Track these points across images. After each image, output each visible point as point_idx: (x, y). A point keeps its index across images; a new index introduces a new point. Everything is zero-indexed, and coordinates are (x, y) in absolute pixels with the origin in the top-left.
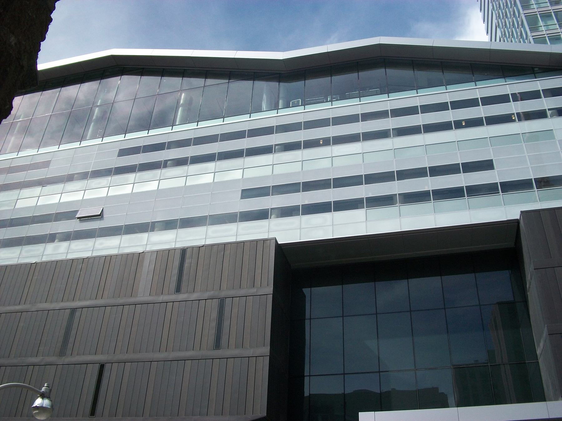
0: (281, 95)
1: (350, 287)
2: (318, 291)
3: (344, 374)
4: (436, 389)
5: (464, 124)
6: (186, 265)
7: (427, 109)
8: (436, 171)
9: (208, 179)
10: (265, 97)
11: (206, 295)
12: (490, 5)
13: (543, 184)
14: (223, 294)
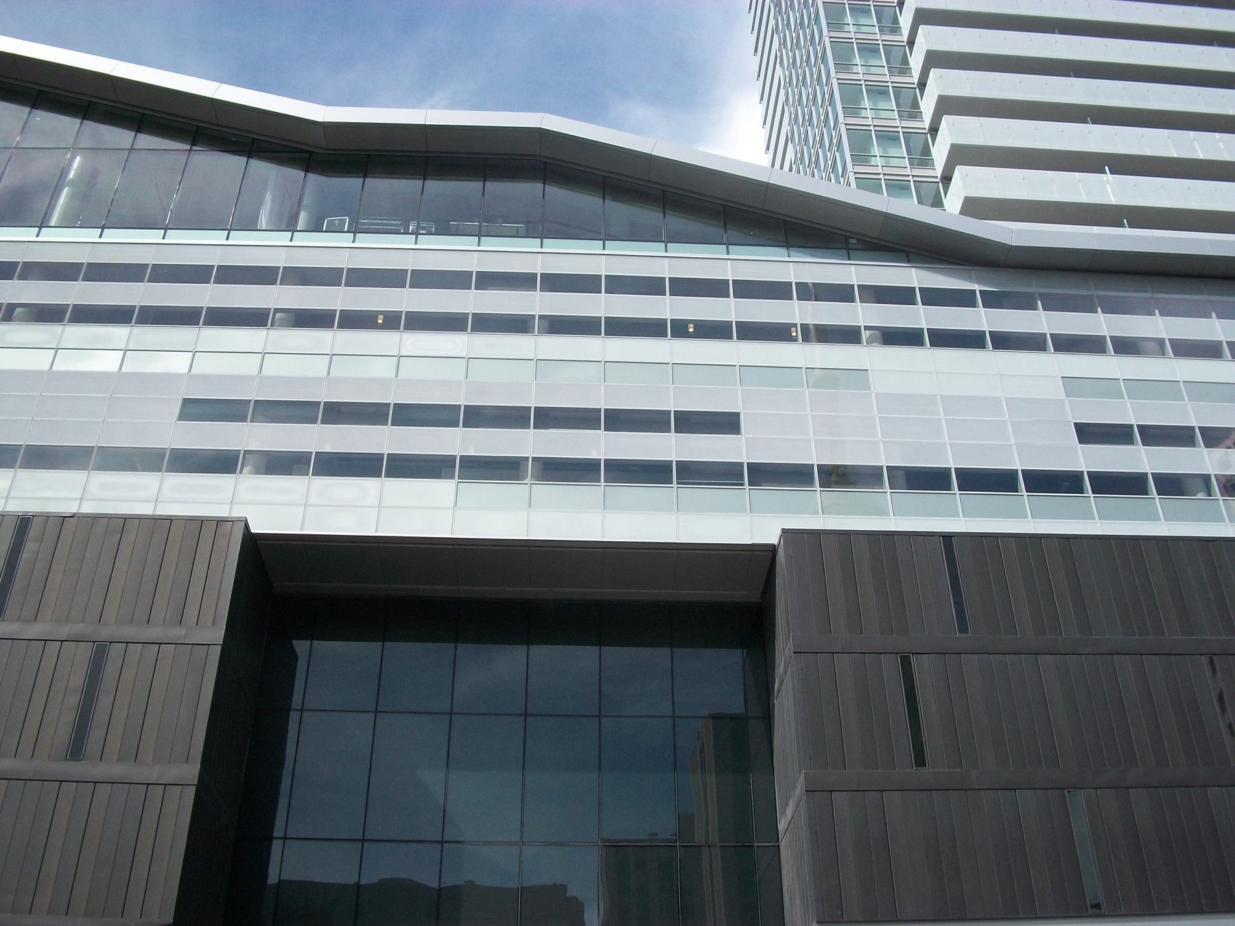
0: (307, 201)
1: (397, 649)
2: (326, 648)
3: (363, 840)
4: (564, 888)
5: (691, 330)
6: (26, 555)
7: (619, 285)
8: (619, 420)
9: (107, 362)
10: (268, 197)
11: (64, 631)
12: (782, 92)
13: (834, 478)
14: (105, 633)
